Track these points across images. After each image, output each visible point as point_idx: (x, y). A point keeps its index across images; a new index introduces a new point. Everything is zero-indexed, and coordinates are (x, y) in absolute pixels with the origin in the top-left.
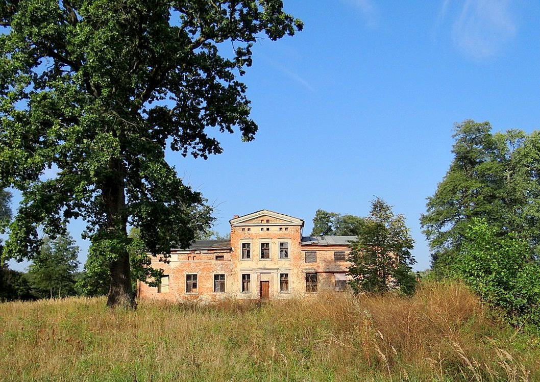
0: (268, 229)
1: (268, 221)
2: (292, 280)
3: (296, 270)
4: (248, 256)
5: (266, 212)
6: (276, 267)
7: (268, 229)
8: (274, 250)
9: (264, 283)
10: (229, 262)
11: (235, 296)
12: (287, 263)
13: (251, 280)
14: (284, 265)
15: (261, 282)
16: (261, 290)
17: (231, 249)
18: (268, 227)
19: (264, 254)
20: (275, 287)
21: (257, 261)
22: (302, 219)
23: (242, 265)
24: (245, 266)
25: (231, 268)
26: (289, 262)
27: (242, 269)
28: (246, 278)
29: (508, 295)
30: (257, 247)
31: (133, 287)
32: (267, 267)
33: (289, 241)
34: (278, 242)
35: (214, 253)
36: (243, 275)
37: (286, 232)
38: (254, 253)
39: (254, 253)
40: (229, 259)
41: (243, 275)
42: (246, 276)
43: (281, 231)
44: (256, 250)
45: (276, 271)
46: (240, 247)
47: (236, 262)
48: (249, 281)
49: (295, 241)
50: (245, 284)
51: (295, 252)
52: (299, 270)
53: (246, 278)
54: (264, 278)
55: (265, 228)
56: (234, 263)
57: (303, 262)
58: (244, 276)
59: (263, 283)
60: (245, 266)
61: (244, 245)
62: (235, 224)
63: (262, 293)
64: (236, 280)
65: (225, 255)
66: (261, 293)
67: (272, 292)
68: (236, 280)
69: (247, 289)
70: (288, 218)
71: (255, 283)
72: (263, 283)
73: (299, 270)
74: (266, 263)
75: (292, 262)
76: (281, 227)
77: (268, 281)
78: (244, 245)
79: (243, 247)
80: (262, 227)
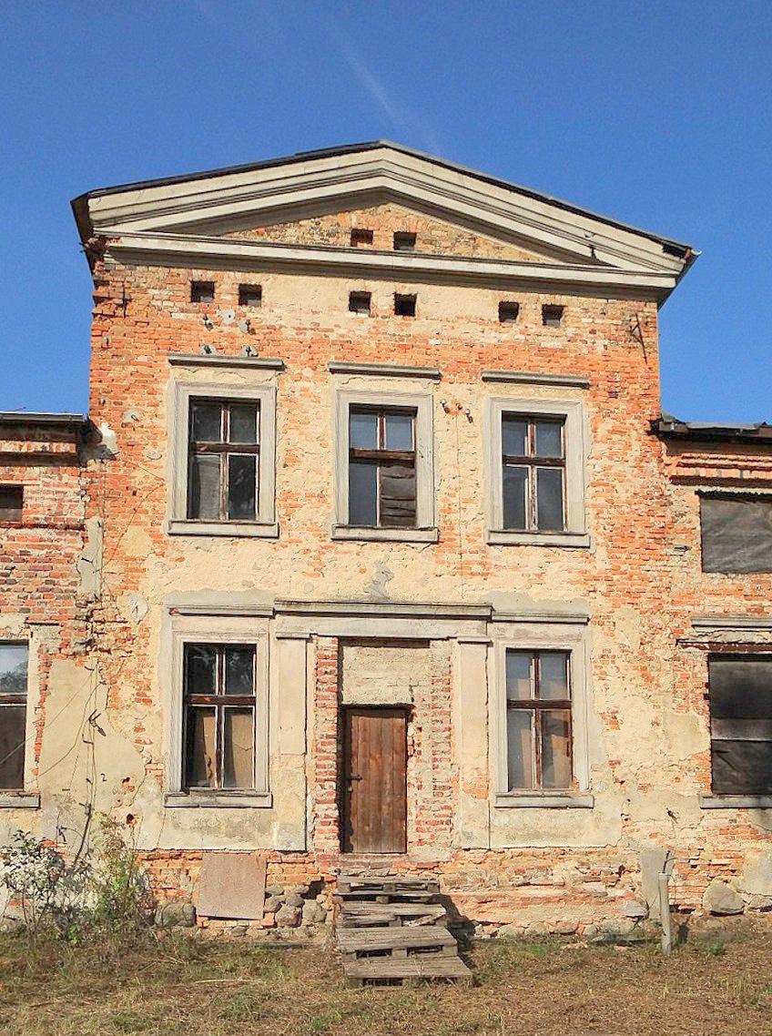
0: (405, 306)
1: (404, 240)
2: (603, 704)
3: (629, 628)
4: (242, 497)
5: (392, 166)
6: (472, 592)
7: (405, 306)
8: (459, 462)
9: (374, 722)
10: (70, 543)
11: (109, 824)
12: (554, 567)
13: (260, 694)
14: (533, 578)
15: (346, 713)
16: (344, 778)
17: (84, 434)
18: (406, 289)
19: (382, 487)
20: (464, 743)
21: (313, 544)
22: (680, 241)
23: (182, 569)
24: (192, 579)
25: (86, 589)
26: (572, 560)
27: (183, 602)
28: (216, 679)
29: (469, 572)
30: (317, 428)
31: (478, 234)
32: (395, 590)
33: (578, 410)
34: (488, 404)
35: (347, 364)
36: (189, 648)
37: (551, 338)
38: (292, 479)
39: (292, 479)
40: (74, 514)
41: (189, 648)
42: (219, 662)
43: (512, 332)
44: (305, 453)
45: (471, 629)
46: (165, 423)
47: (136, 541)
48: (245, 707)
49: (621, 405)
50: (210, 726)
51: (623, 494)
52: (657, 630)
53: (216, 679)
54: (374, 680)
55: (383, 294)
56: (113, 552)
57: (685, 572)
58: (197, 660)
59: (358, 722)
60: (192, 579)
61: (204, 410)
62: (129, 235)
63: (356, 802)
64: (127, 692)
65: (34, 480)
66: (343, 800)
67: (438, 790)
68: (127, 692)
69: (229, 774)
70: (570, 230)
71: (293, 720)
72: (358, 722)
73: (657, 630)
74: (405, 570)
75: (601, 561)
76: (511, 296)
77: (405, 711)
78: (204, 410)
79: (196, 430)
80: (358, 285)
